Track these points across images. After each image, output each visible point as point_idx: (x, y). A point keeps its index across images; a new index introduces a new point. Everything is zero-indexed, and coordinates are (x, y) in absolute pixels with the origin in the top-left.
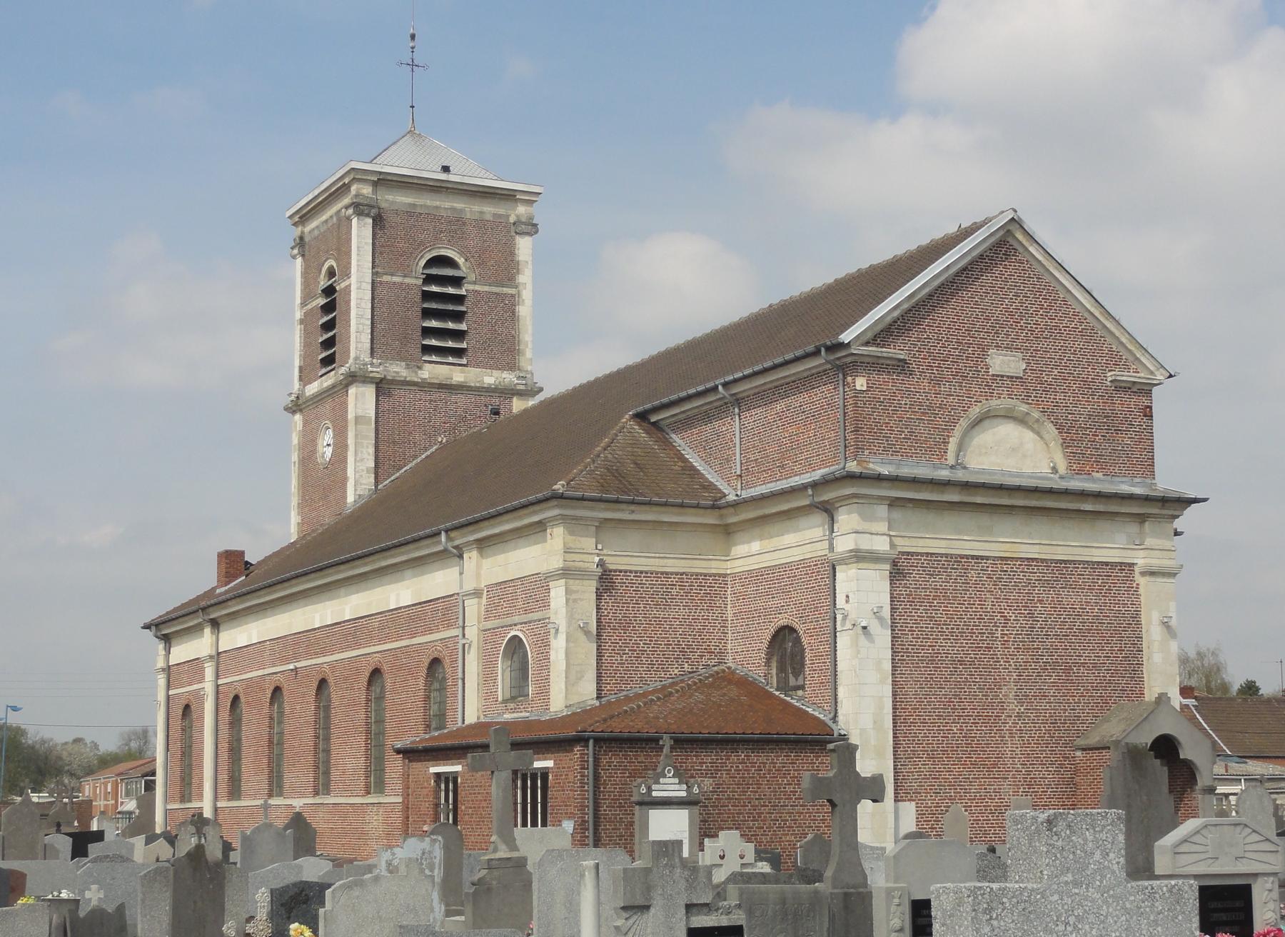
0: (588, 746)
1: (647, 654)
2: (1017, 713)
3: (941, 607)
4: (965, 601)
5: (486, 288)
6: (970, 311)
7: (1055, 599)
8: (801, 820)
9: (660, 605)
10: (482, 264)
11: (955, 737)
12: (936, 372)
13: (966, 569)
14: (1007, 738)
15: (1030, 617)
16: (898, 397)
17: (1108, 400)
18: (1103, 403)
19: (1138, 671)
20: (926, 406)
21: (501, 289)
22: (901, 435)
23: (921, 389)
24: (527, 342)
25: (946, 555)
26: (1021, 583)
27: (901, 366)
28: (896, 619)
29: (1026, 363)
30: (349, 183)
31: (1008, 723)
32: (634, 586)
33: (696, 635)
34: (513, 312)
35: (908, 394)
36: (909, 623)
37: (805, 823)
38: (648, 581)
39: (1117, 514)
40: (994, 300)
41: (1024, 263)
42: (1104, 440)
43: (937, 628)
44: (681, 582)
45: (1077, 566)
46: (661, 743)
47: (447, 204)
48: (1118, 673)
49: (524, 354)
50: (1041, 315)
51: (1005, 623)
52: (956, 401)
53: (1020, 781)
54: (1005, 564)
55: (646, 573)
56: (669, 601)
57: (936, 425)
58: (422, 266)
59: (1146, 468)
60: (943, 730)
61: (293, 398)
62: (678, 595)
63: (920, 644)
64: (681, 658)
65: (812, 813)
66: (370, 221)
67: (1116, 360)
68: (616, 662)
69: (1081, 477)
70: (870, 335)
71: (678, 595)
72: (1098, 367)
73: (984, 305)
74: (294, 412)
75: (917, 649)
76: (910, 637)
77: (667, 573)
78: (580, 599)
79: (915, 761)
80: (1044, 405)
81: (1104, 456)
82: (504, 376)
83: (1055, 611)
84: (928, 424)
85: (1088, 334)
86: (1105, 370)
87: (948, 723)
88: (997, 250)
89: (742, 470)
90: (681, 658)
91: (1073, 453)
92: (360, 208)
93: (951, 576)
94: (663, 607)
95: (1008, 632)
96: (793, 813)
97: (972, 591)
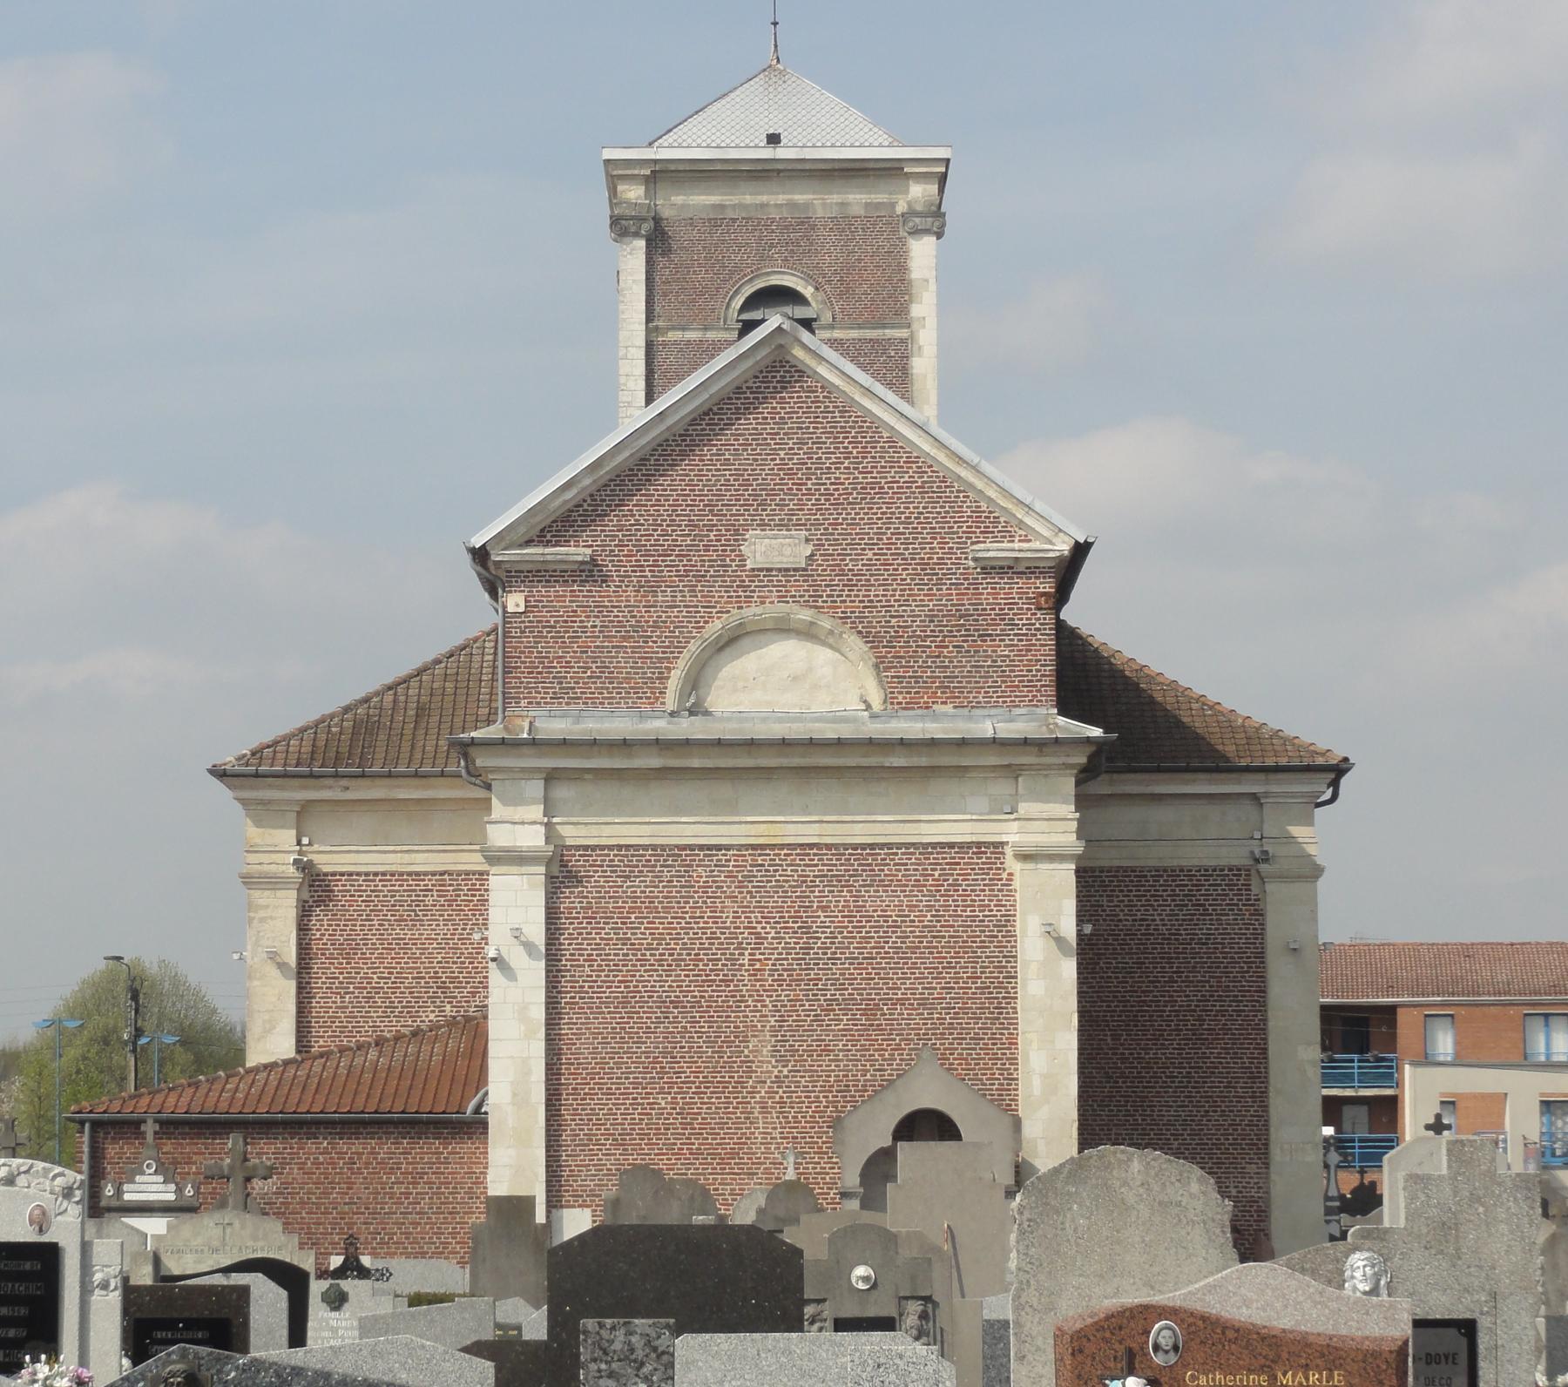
2: (776, 1077)
3: (643, 923)
4: (687, 912)
6: (713, 476)
7: (852, 904)
9: (406, 920)
10: (845, 292)
11: (663, 1114)
13: (688, 866)
14: (756, 1115)
15: (802, 933)
17: (969, 589)
20: (630, 626)
21: (880, 332)
22: (586, 672)
23: (622, 601)
25: (654, 847)
27: (589, 572)
28: (564, 944)
29: (814, 545)
31: (760, 1092)
32: (364, 894)
33: (464, 963)
35: (599, 612)
36: (587, 950)
37: (422, 1238)
38: (386, 886)
40: (761, 455)
41: (817, 392)
44: (440, 885)
45: (895, 851)
47: (781, 196)
50: (845, 468)
51: (755, 944)
52: (684, 614)
54: (760, 855)
55: (384, 874)
56: (420, 913)
57: (645, 653)
58: (738, 307)
59: (1039, 691)
60: (643, 1104)
62: (435, 905)
63: (603, 978)
64: (440, 997)
67: (990, 523)
68: (334, 1005)
69: (911, 713)
71: (435, 905)
73: (739, 464)
75: (598, 987)
76: (587, 969)
77: (417, 874)
79: (593, 1150)
84: (632, 652)
85: (935, 489)
90: (440, 997)
91: (898, 677)
93: (662, 876)
94: (410, 923)
95: (762, 957)
97: (699, 897)
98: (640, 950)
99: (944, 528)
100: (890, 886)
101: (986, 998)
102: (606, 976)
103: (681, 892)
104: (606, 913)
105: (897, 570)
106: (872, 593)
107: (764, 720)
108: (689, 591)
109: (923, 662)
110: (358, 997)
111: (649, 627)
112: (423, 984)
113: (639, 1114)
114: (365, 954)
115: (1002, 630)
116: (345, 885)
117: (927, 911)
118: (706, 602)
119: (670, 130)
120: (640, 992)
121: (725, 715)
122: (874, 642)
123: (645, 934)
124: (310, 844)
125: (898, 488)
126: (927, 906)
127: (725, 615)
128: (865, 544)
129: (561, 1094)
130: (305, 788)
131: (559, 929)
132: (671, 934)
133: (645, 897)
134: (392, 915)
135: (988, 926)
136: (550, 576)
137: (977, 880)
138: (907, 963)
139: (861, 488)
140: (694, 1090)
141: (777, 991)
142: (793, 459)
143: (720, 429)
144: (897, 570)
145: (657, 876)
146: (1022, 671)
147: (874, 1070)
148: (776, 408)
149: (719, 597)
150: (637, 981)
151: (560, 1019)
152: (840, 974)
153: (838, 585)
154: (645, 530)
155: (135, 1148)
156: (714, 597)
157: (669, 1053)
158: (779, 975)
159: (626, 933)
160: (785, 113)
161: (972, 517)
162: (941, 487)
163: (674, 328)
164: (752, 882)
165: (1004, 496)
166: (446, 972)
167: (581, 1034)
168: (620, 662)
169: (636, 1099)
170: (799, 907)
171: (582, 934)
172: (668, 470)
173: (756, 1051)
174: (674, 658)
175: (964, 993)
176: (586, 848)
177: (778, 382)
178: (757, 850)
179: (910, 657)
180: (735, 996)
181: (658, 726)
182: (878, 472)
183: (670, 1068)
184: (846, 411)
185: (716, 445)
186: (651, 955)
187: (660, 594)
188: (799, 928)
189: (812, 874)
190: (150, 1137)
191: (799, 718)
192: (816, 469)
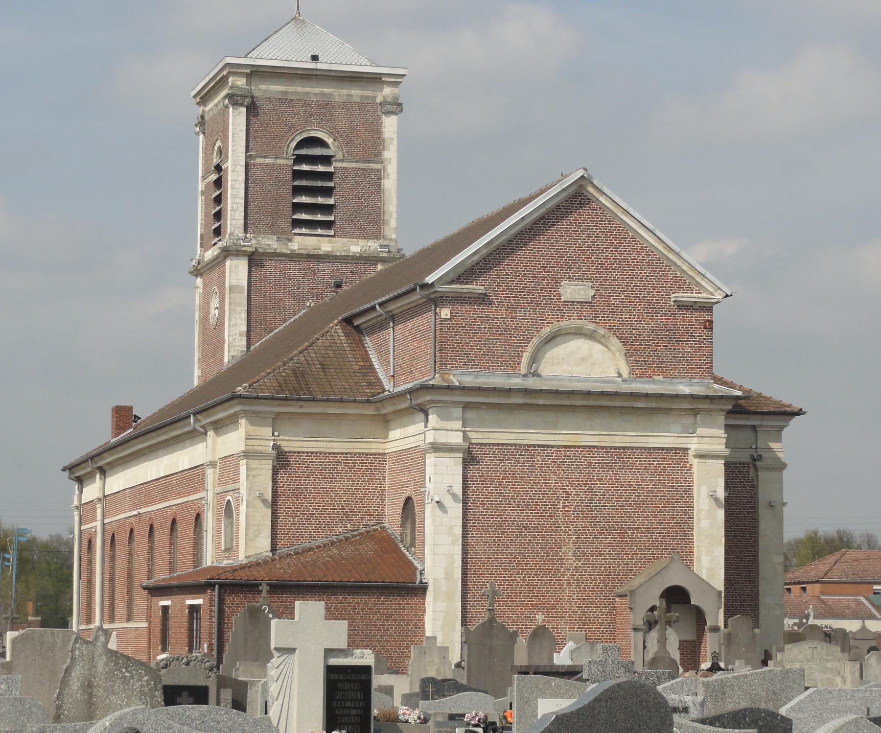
0: (215, 590)
1: (316, 517)
2: (575, 567)
3: (509, 485)
4: (532, 480)
5: (354, 165)
6: (545, 251)
7: (613, 478)
8: (388, 646)
9: (328, 478)
10: (349, 142)
11: (518, 585)
12: (513, 301)
14: (565, 586)
15: (589, 492)
16: (478, 322)
18: (665, 319)
19: (688, 534)
20: (503, 328)
21: (367, 165)
22: (480, 352)
23: (499, 315)
24: (391, 212)
25: (515, 445)
26: (582, 465)
27: (483, 299)
29: (595, 290)
30: (227, 75)
31: (567, 575)
32: (306, 463)
33: (357, 502)
34: (379, 186)
36: (481, 498)
37: (391, 649)
38: (317, 459)
39: (671, 409)
40: (569, 241)
42: (666, 349)
43: (505, 501)
44: (345, 460)
45: (635, 451)
46: (260, 588)
47: (317, 89)
48: (669, 536)
49: (388, 224)
50: (611, 251)
51: (566, 497)
53: (575, 620)
54: (568, 451)
55: (316, 453)
56: (335, 475)
57: (511, 343)
58: (293, 147)
60: (508, 580)
61: (194, 263)
64: (344, 520)
65: (398, 641)
66: (244, 110)
67: (682, 282)
69: (642, 379)
70: (452, 276)
71: (343, 471)
72: (663, 290)
74: (196, 276)
75: (487, 518)
76: (481, 508)
77: (334, 453)
78: (258, 475)
80: (611, 323)
81: (665, 362)
82: (369, 244)
83: (613, 487)
84: (504, 342)
86: (670, 293)
87: (513, 575)
88: (572, 201)
89: (394, 372)
90: (344, 520)
92: (234, 99)
96: (381, 641)
97: (538, 472)
98: (508, 499)
99: (659, 284)
100: (632, 469)
101: (678, 528)
102: (491, 512)
103: (528, 469)
104: (491, 479)
105: (636, 305)
106: (623, 317)
107: (570, 380)
108: (533, 311)
109: (649, 353)
110: (302, 519)
111: (512, 329)
112: (336, 513)
113: (507, 585)
114: (306, 495)
115: (687, 338)
116: (296, 458)
117: (650, 483)
118: (541, 317)
119: (254, 49)
120: (508, 521)
121: (548, 377)
122: (624, 342)
123: (510, 491)
124: (278, 436)
125: (637, 262)
126: (650, 480)
127: (551, 325)
128: (621, 291)
129: (467, 574)
130: (280, 405)
131: (468, 487)
132: (524, 491)
133: (511, 471)
134: (320, 475)
135: (680, 491)
136: (463, 300)
137: (674, 467)
138: (640, 509)
139: (619, 262)
140: (534, 573)
141: (576, 522)
142: (585, 245)
143: (549, 227)
144: (636, 305)
145: (517, 461)
146: (696, 360)
147: (624, 564)
148: (576, 218)
149: (548, 315)
150: (506, 515)
151: (467, 534)
152: (608, 514)
153: (607, 312)
154: (511, 278)
155: (241, 599)
156: (545, 315)
157: (522, 553)
158: (577, 514)
159: (501, 490)
160: (311, 44)
161: (672, 279)
162: (657, 263)
163: (259, 156)
164: (564, 465)
165: (691, 270)
166: (348, 507)
167: (478, 542)
168: (498, 347)
169: (505, 577)
170: (588, 478)
171: (479, 490)
172: (522, 247)
173: (566, 553)
174: (525, 346)
175: (668, 526)
176: (481, 444)
177: (578, 204)
178: (566, 448)
179: (642, 350)
180: (555, 524)
181: (516, 382)
182: (627, 254)
183: (522, 561)
184: (611, 221)
185: (547, 235)
186: (514, 502)
187: (518, 312)
188: (587, 489)
189: (594, 461)
190: (264, 593)
191: (586, 380)
192: (596, 250)
